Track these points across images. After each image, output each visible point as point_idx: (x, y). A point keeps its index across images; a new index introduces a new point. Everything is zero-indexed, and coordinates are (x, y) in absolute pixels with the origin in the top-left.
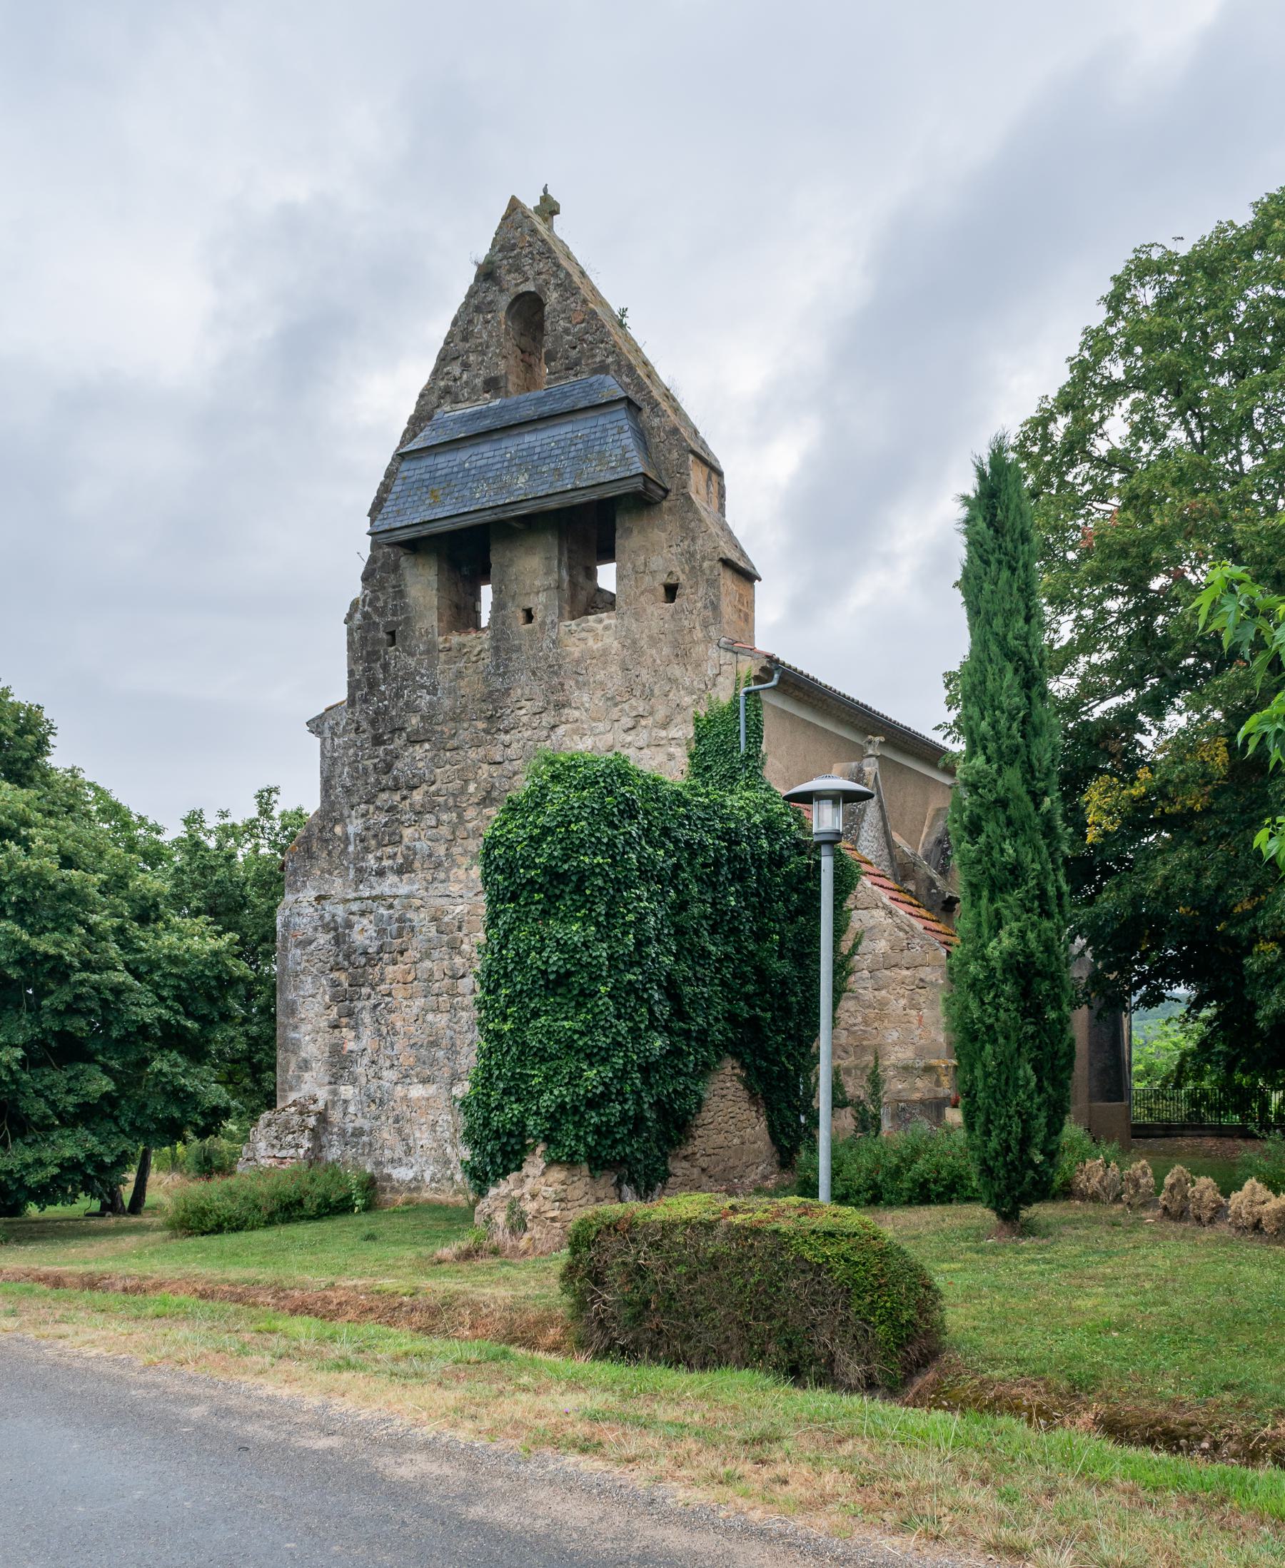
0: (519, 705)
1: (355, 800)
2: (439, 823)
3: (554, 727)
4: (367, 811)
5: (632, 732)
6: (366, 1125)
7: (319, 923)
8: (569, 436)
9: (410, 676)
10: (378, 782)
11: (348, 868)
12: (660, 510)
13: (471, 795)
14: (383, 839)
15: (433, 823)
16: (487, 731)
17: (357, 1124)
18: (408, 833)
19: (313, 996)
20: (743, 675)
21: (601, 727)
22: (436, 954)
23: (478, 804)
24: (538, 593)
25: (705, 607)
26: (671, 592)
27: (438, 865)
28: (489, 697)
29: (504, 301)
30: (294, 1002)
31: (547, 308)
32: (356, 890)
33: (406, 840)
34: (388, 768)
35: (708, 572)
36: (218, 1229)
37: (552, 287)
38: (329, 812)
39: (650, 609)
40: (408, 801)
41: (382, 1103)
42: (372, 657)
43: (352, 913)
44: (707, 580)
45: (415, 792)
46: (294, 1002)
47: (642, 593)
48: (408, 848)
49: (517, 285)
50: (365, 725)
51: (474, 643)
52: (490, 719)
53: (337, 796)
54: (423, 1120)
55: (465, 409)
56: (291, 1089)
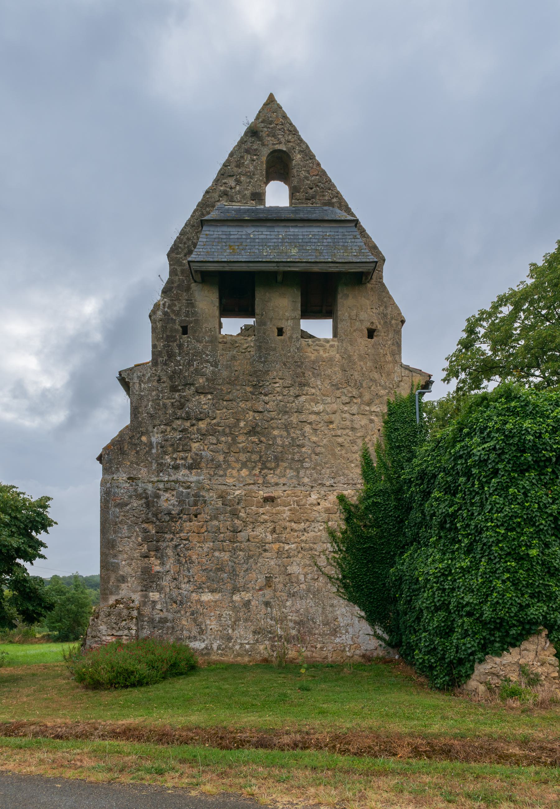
0: (274, 381)
1: (157, 422)
2: (219, 442)
3: (297, 396)
4: (166, 430)
5: (347, 405)
6: (170, 616)
7: (134, 493)
8: (321, 233)
9: (198, 354)
10: (174, 413)
11: (151, 463)
12: (366, 288)
13: (242, 428)
14: (178, 448)
15: (215, 442)
16: (252, 393)
17: (162, 615)
18: (195, 446)
19: (129, 537)
20: (415, 383)
21: (329, 400)
22: (221, 517)
23: (246, 434)
24: (287, 320)
25: (393, 344)
26: (371, 333)
27: (218, 466)
28: (254, 373)
29: (265, 152)
30: (114, 540)
31: (294, 162)
32: (158, 476)
33: (194, 450)
34: (182, 406)
35: (395, 326)
36: (140, 683)
37: (297, 152)
38: (137, 427)
39: (359, 340)
40: (195, 427)
41: (181, 603)
42: (170, 339)
43: (159, 489)
44: (394, 330)
45: (200, 423)
46: (114, 540)
47: (355, 331)
48: (197, 454)
49: (273, 144)
50: (164, 378)
51: (243, 342)
52: (254, 386)
53: (143, 419)
54: (212, 614)
55: (236, 206)
56: (111, 593)
